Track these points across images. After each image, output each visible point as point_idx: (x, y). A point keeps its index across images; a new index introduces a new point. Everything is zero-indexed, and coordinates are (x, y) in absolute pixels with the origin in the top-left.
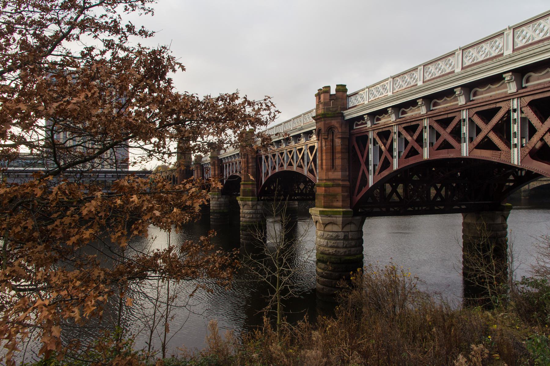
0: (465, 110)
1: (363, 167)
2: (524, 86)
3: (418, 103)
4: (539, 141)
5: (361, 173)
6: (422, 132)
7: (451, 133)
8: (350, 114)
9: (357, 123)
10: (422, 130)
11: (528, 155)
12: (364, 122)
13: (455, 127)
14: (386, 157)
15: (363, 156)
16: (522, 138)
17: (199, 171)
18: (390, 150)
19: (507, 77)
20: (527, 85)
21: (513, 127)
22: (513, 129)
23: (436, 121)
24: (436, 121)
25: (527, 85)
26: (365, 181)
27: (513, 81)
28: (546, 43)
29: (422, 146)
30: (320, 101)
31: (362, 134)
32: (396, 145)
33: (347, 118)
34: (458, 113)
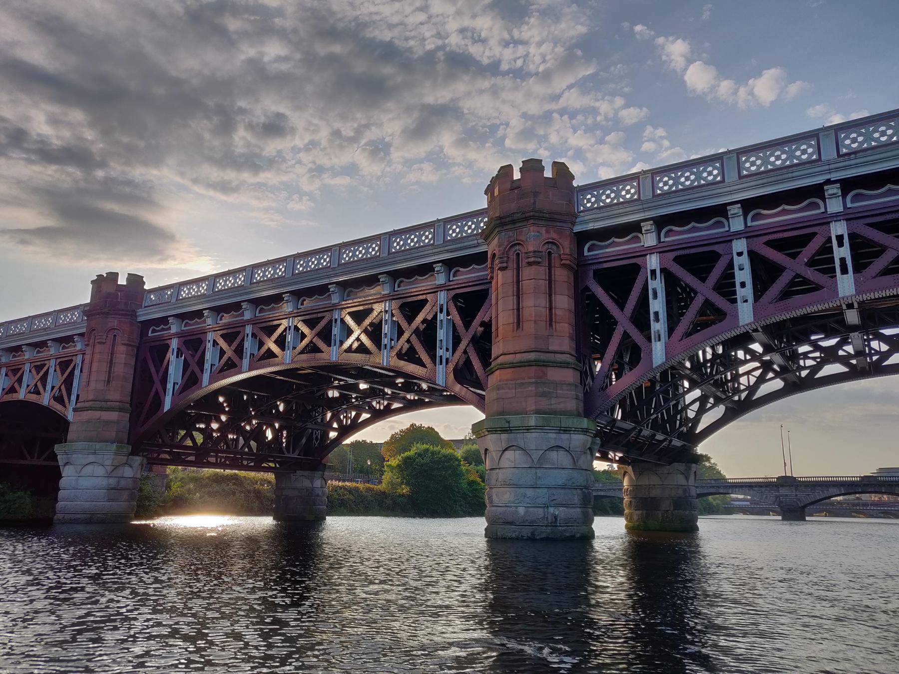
0: (388, 302)
1: (158, 385)
2: (451, 279)
3: (284, 298)
4: (406, 343)
5: (153, 391)
6: (243, 340)
7: (276, 342)
8: (144, 315)
9: (64, 346)
10: (244, 338)
11: (471, 345)
12: (73, 344)
13: (324, 328)
14: (193, 371)
15: (158, 372)
16: (392, 340)
17: (121, 349)
18: (201, 363)
19: (438, 267)
20: (455, 279)
21: (385, 327)
22: (385, 329)
23: (261, 328)
24: (261, 328)
25: (455, 279)
26: (158, 402)
27: (653, 232)
28: (897, 145)
29: (241, 358)
30: (100, 291)
31: (161, 343)
32: (208, 356)
33: (140, 319)
34: (241, 328)
